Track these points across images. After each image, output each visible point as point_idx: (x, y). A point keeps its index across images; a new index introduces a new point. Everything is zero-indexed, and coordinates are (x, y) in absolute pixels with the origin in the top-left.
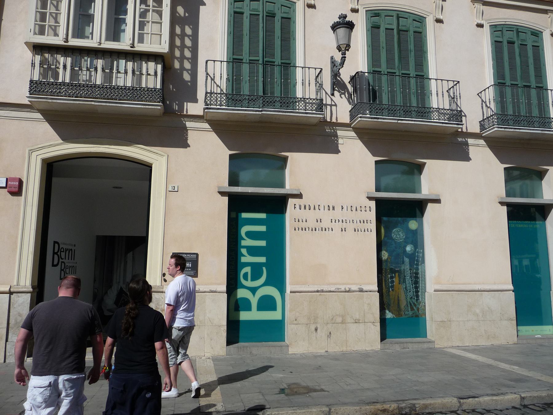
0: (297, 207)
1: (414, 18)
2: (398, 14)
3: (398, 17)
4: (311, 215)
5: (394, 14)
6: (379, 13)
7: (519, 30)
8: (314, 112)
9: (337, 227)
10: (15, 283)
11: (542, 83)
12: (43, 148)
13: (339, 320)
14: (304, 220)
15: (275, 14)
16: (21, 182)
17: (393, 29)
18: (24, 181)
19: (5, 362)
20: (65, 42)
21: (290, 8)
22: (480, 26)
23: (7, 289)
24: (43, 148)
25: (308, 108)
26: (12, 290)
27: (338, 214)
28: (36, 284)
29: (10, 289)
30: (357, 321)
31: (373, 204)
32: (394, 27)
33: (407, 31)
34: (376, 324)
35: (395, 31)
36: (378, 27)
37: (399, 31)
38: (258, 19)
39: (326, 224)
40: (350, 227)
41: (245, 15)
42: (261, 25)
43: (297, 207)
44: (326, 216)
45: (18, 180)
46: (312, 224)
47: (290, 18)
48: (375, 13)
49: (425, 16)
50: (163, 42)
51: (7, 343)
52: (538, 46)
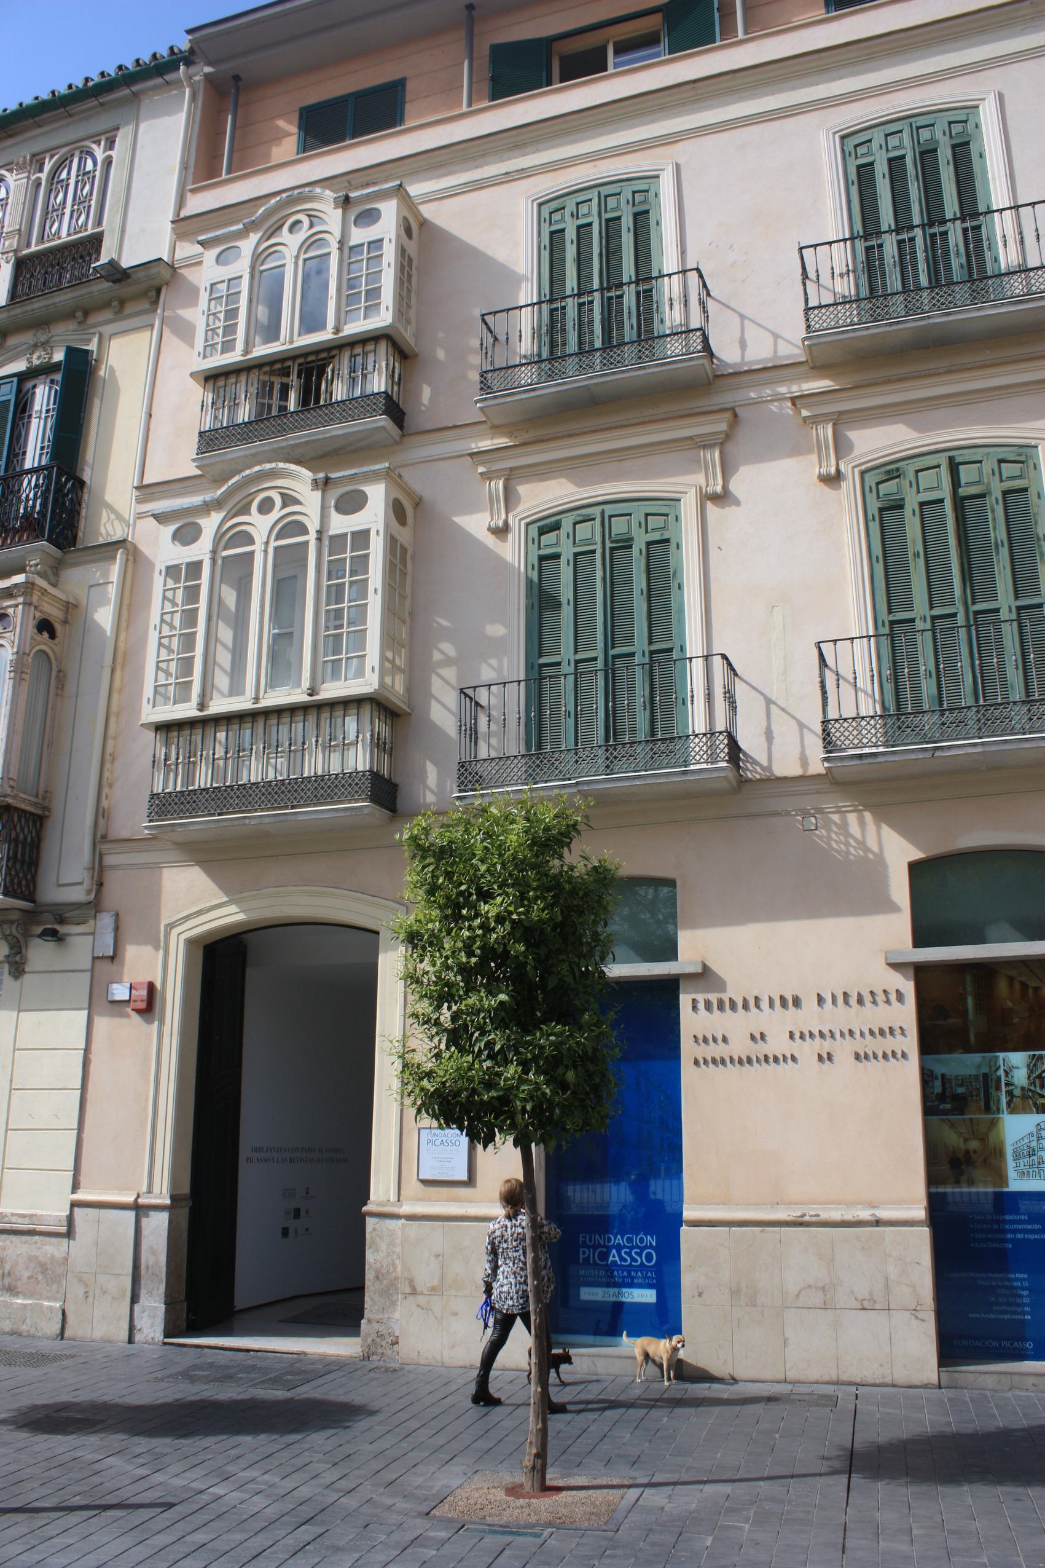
0: (701, 1005)
1: (1001, 457)
2: (951, 459)
3: (954, 467)
4: (736, 1027)
5: (943, 460)
6: (897, 469)
7: (958, 460)
8: (881, 749)
9: (807, 1050)
10: (145, 1189)
11: (669, 637)
12: (187, 918)
13: (817, 1299)
14: (720, 1038)
15: (632, 539)
16: (151, 987)
17: (942, 501)
18: (158, 985)
19: (131, 1340)
20: (310, 695)
21: (667, 515)
22: (833, 480)
23: (129, 1199)
24: (187, 918)
25: (865, 741)
26: (141, 1201)
27: (809, 1017)
28: (186, 1189)
29: (136, 1200)
30: (866, 1304)
31: (909, 988)
32: (946, 492)
33: (983, 496)
34: (921, 1315)
35: (948, 505)
36: (899, 506)
37: (959, 503)
38: (593, 561)
39: (778, 1044)
40: (844, 1049)
41: (563, 560)
42: (599, 574)
43: (701, 1005)
44: (777, 1025)
45: (146, 986)
46: (739, 1047)
47: (667, 541)
48: (888, 472)
49: (676, 496)
50: (368, 669)
51: (137, 1307)
52: (1025, 490)
